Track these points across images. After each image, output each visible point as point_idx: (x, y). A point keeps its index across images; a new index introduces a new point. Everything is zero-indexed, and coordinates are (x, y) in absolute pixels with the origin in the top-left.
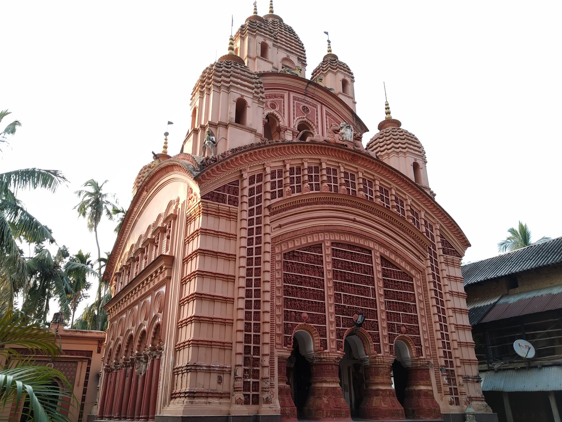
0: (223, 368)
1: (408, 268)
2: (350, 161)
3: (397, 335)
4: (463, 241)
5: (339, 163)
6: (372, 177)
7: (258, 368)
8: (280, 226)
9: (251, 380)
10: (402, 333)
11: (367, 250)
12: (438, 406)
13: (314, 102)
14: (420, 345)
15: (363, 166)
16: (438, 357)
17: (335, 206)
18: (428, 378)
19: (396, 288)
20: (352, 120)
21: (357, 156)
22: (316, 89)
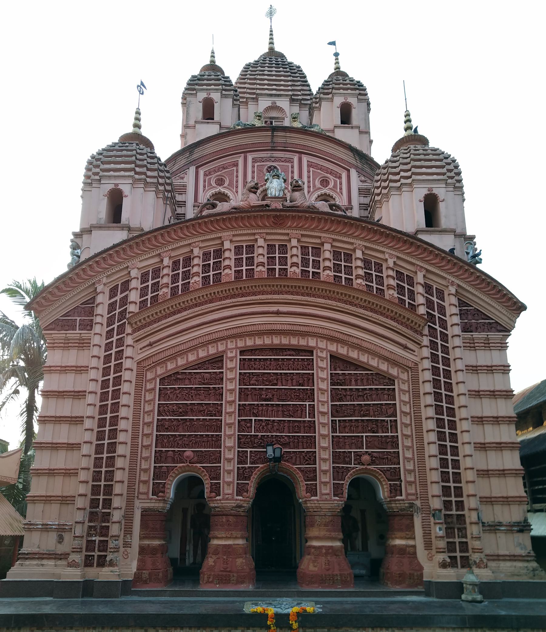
0: (64, 525)
1: (384, 367)
2: (272, 227)
3: (353, 468)
4: (509, 304)
5: (254, 234)
6: (318, 241)
7: (107, 524)
8: (150, 345)
9: (97, 539)
10: (363, 464)
11: (305, 351)
12: (421, 568)
13: (288, 155)
14: (400, 479)
15: (296, 228)
16: (430, 496)
17: (243, 299)
18: (411, 527)
19: (361, 398)
20: (354, 162)
21: (280, 215)
22: (288, 134)
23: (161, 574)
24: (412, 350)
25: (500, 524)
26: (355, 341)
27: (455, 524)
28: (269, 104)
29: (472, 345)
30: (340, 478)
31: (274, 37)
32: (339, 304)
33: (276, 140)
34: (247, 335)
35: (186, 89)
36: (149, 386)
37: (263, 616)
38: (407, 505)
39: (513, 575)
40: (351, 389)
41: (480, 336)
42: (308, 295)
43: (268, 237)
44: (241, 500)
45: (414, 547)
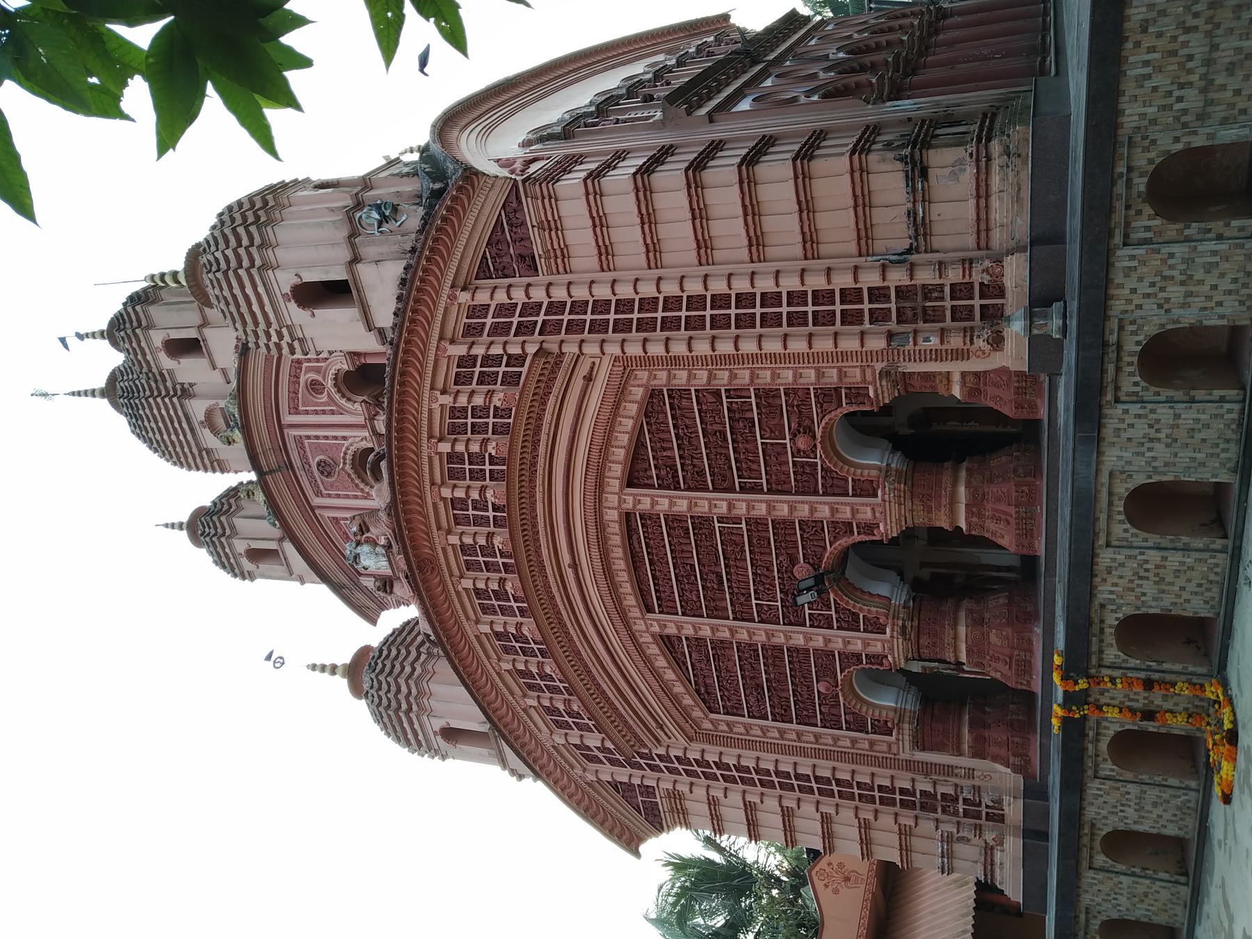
1: (632, 409)
10: (815, 446)
11: (628, 526)
12: (1003, 371)
13: (291, 445)
15: (430, 539)
21: (419, 567)
22: (259, 450)
23: (1017, 740)
24: (592, 368)
25: (912, 214)
26: (595, 454)
27: (916, 307)
28: (207, 432)
29: (559, 253)
30: (842, 483)
31: (82, 389)
32: (539, 482)
33: (274, 466)
34: (621, 603)
35: (206, 470)
36: (724, 727)
37: (1065, 721)
38: (884, 383)
39: (1018, 199)
40: (681, 457)
41: (539, 241)
42: (535, 525)
43: (456, 572)
44: (893, 630)
45: (964, 375)
